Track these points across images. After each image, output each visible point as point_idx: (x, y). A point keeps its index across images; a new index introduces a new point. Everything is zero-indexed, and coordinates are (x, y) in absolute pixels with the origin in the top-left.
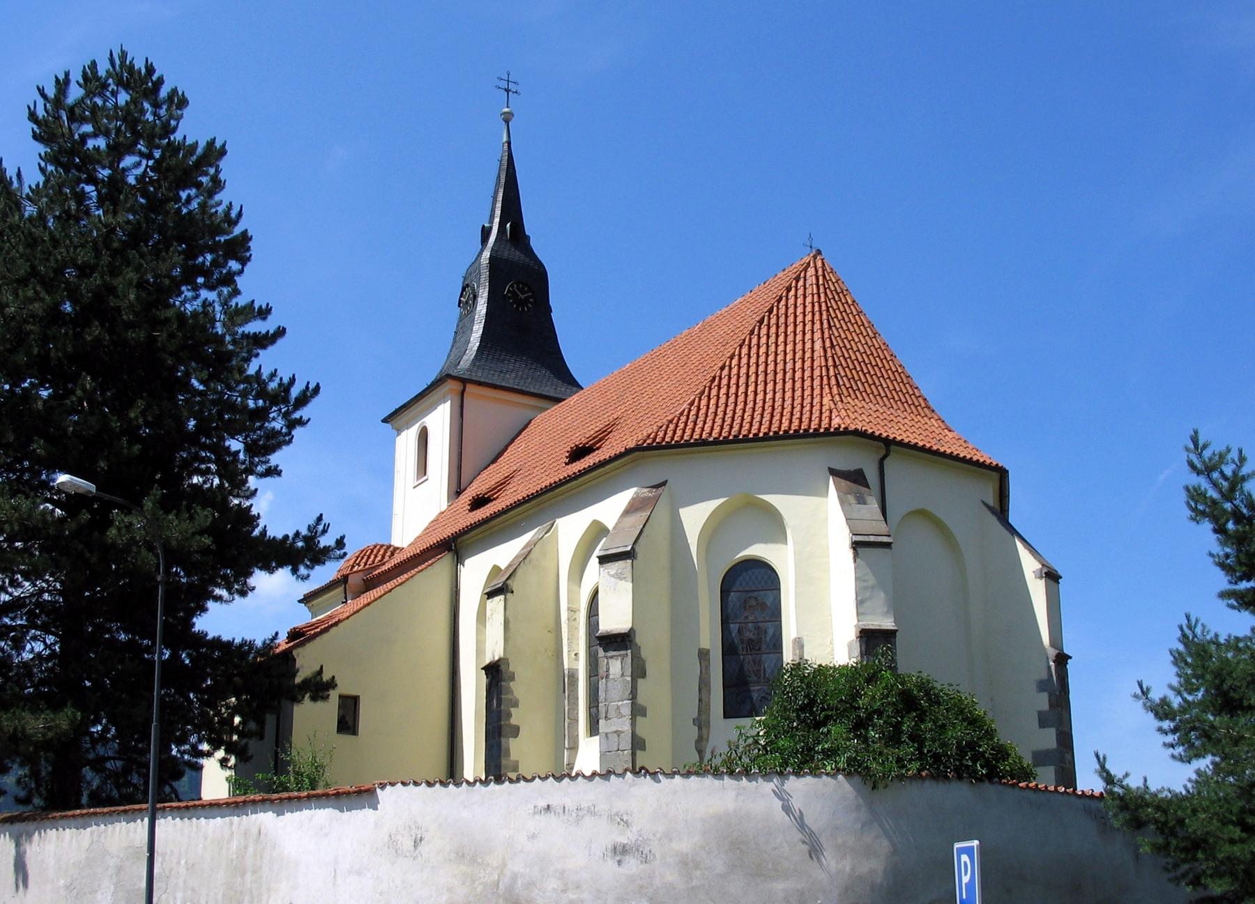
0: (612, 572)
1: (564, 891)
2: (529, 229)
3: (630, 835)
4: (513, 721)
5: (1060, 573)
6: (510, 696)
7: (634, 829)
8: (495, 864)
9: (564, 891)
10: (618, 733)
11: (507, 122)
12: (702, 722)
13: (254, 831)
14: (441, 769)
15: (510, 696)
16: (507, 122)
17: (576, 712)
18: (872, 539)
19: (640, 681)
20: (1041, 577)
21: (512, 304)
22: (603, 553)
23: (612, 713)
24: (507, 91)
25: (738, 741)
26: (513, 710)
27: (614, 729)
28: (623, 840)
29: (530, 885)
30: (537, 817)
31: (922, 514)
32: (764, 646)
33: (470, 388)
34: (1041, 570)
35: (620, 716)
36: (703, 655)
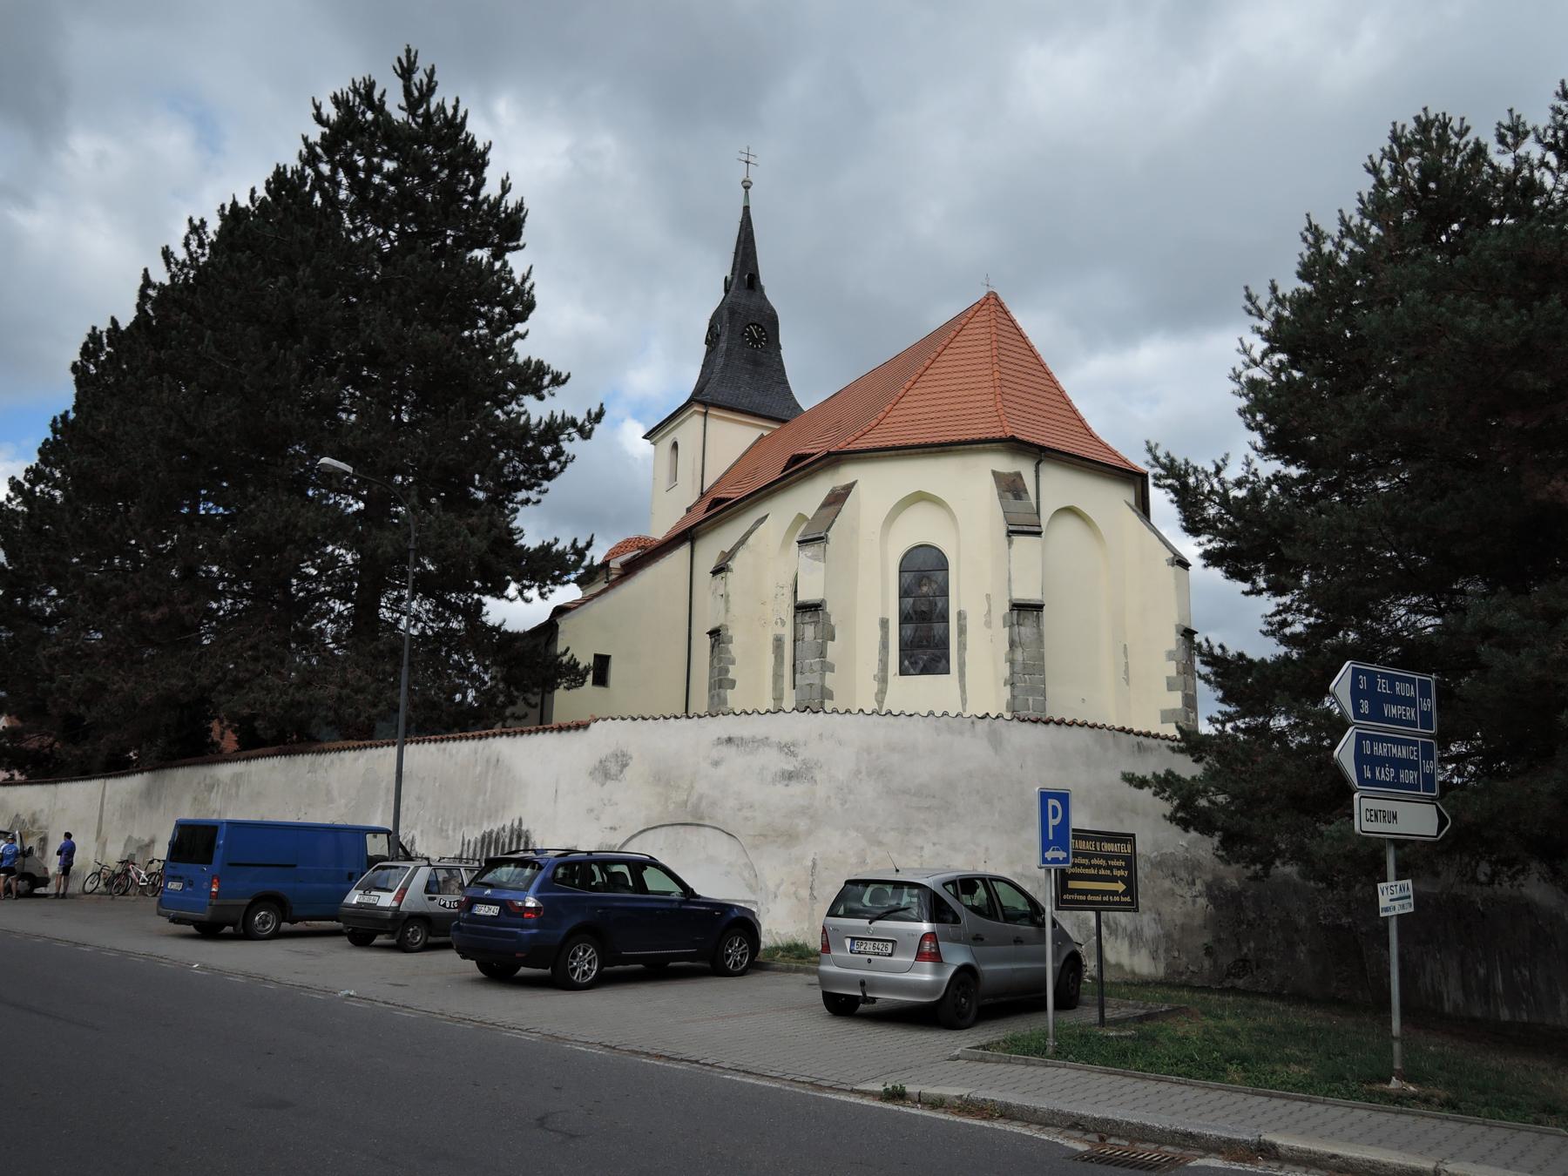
0: (809, 554)
1: (740, 810)
2: (764, 278)
3: (796, 764)
4: (730, 676)
5: (1190, 562)
6: (728, 656)
7: (799, 758)
8: (686, 787)
9: (740, 810)
10: (811, 685)
11: (747, 188)
12: (883, 680)
13: (493, 760)
14: (680, 710)
15: (728, 656)
16: (747, 188)
17: (1019, 656)
18: (1026, 529)
19: (829, 643)
20: (1173, 565)
21: (748, 342)
22: (801, 539)
23: (807, 668)
24: (747, 162)
25: (222, 733)
26: (731, 667)
27: (808, 682)
28: (790, 768)
29: (713, 804)
30: (720, 747)
31: (1070, 511)
32: (934, 617)
33: (712, 411)
34: (1173, 559)
35: (812, 671)
36: (884, 623)
